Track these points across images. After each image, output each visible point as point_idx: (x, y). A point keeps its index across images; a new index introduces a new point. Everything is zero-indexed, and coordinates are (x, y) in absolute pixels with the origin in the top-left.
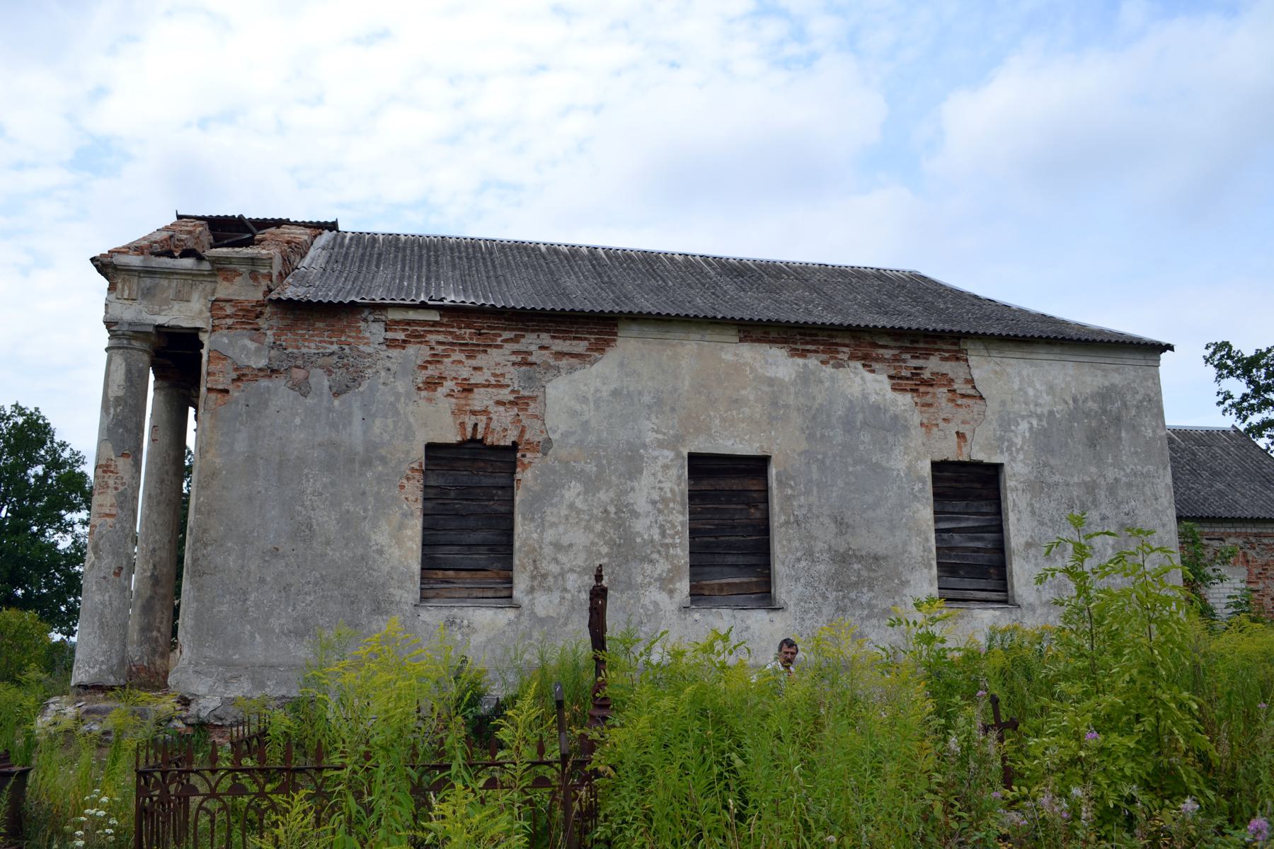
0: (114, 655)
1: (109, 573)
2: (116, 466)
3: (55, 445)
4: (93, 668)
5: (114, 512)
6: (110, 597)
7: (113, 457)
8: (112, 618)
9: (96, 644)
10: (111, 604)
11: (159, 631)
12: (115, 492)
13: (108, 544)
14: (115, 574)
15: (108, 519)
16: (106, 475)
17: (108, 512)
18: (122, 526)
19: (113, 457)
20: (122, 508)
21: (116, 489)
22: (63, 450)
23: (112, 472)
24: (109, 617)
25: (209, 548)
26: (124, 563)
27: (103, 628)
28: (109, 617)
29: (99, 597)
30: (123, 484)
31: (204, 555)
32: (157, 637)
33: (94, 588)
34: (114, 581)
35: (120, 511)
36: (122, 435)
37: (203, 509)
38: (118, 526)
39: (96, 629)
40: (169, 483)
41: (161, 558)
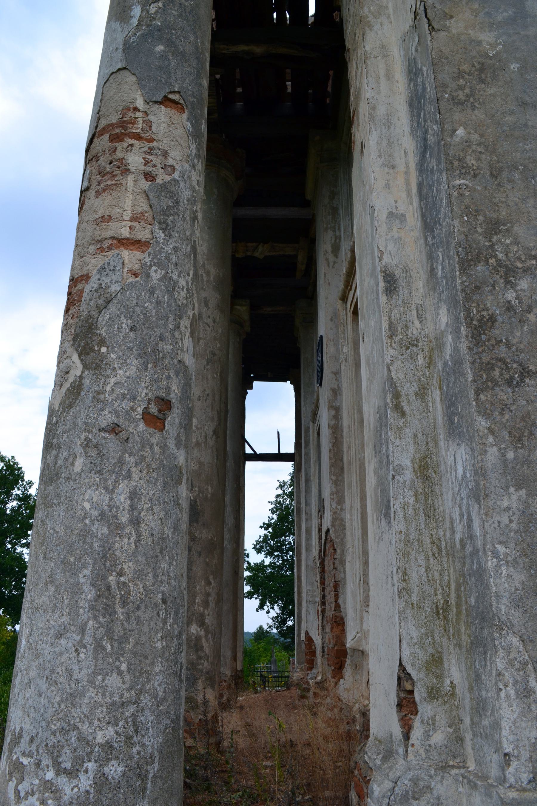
0: (148, 717)
1: (128, 414)
2: (149, 124)
3: (25, 484)
4: (72, 774)
5: (144, 235)
6: (134, 495)
7: (140, 103)
8: (139, 575)
9: (82, 675)
10: (136, 522)
11: (202, 624)
12: (145, 185)
13: (125, 324)
14: (147, 417)
15: (125, 254)
16: (121, 146)
17: (125, 233)
18: (166, 278)
19: (140, 103)
20: (166, 228)
21: (149, 176)
22: (30, 487)
23: (138, 137)
24: (129, 567)
25: (524, 284)
26: (175, 389)
27: (109, 611)
28: (129, 567)
29: (96, 495)
30: (169, 169)
31: (509, 307)
32: (198, 639)
33: (79, 465)
34: (145, 444)
35: (160, 235)
36: (163, 56)
37: (471, 161)
38: (156, 274)
39: (84, 614)
40: (210, 321)
41: (200, 464)
